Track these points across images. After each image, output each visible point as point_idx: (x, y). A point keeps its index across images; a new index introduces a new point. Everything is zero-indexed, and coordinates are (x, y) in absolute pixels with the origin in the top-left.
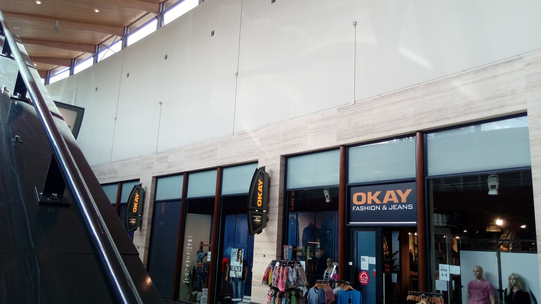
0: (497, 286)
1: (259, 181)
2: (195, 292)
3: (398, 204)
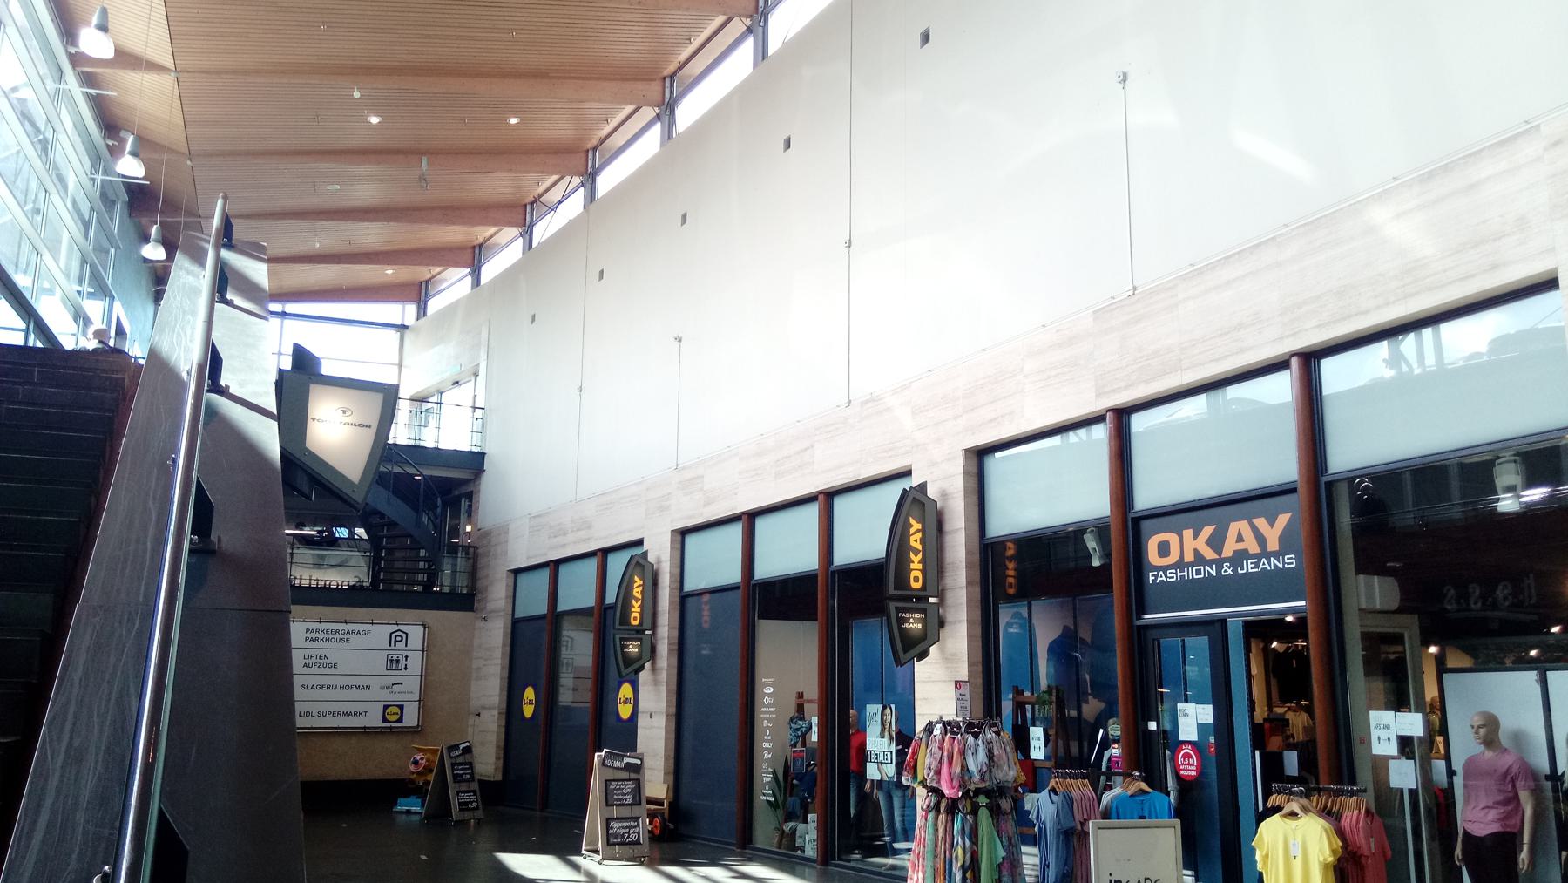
0: (1544, 765)
1: (912, 521)
2: (791, 824)
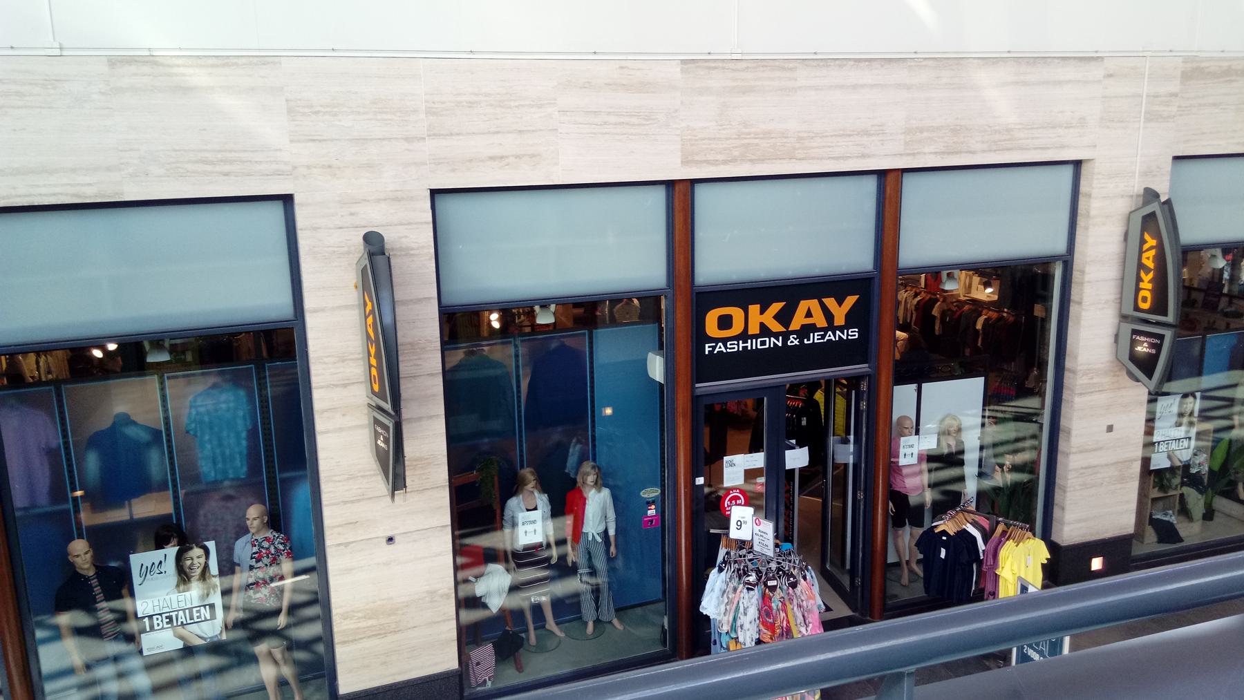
3: (825, 330)
